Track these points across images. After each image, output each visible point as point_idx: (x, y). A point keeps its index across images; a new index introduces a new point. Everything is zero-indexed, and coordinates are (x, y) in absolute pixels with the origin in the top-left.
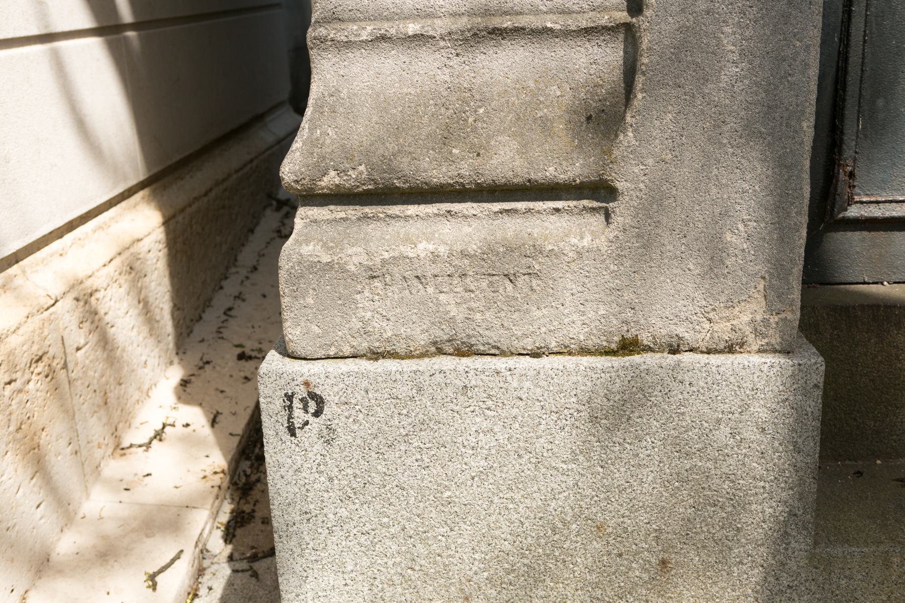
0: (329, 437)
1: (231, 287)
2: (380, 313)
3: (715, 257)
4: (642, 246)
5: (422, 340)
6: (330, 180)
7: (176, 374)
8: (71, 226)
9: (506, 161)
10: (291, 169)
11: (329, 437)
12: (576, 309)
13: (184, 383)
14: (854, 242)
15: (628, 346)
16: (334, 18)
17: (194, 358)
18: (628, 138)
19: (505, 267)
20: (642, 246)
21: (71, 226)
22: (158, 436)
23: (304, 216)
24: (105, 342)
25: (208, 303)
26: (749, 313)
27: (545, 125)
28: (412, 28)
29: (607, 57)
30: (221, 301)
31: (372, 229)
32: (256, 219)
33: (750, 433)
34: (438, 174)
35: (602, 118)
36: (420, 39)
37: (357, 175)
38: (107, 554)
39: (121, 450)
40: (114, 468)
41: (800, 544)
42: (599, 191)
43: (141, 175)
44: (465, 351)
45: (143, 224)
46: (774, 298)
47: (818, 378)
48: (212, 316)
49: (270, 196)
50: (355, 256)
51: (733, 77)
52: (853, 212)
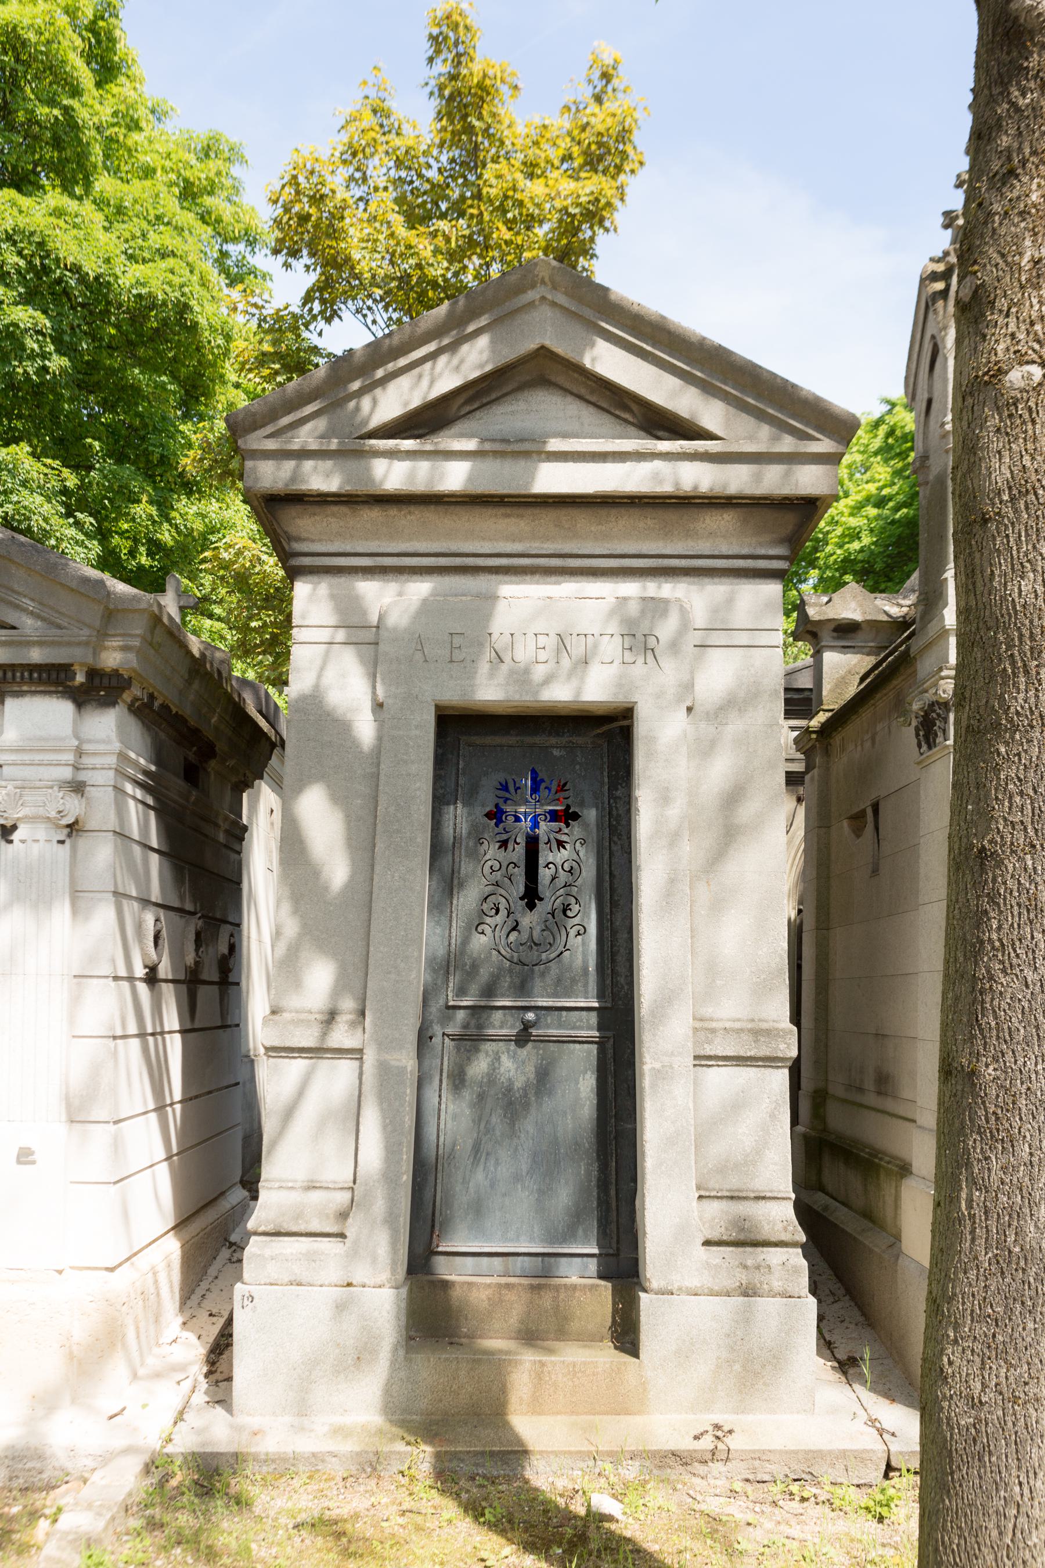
0: (254, 1309)
1: (204, 1285)
2: (272, 1271)
3: (374, 1260)
4: (353, 1254)
5: (286, 1280)
6: (261, 1229)
7: (180, 1320)
8: (150, 1244)
9: (315, 1226)
10: (251, 1225)
11: (254, 1309)
12: (333, 1273)
13: (184, 1324)
14: (440, 1260)
15: (349, 1285)
16: (266, 1181)
17: (188, 1314)
18: (350, 1220)
19: (311, 1257)
20: (353, 1254)
21: (150, 1244)
22: (175, 1341)
23: (253, 1239)
24: (158, 1295)
25: (193, 1292)
26: (384, 1276)
27: (327, 1216)
28: (290, 1185)
29: (347, 1196)
30: (199, 1292)
31: (274, 1244)
32: (218, 1251)
33: (385, 1314)
34: (294, 1229)
35: (343, 1215)
36: (292, 1188)
37: (269, 1228)
38: (157, 1375)
39: (158, 1345)
40: (156, 1350)
41: (401, 1352)
42: (342, 1236)
43: (172, 1224)
44: (299, 1284)
45: (172, 1247)
46: (393, 1271)
47: (404, 1296)
48: (195, 1298)
49: (226, 1240)
50: (268, 1252)
51: (379, 1206)
52: (440, 1249)
